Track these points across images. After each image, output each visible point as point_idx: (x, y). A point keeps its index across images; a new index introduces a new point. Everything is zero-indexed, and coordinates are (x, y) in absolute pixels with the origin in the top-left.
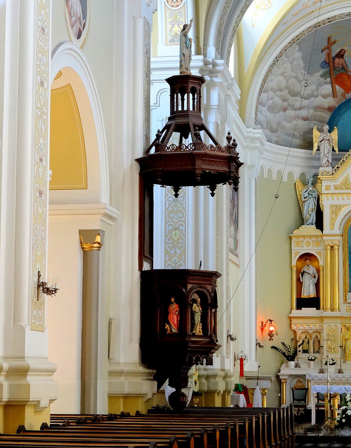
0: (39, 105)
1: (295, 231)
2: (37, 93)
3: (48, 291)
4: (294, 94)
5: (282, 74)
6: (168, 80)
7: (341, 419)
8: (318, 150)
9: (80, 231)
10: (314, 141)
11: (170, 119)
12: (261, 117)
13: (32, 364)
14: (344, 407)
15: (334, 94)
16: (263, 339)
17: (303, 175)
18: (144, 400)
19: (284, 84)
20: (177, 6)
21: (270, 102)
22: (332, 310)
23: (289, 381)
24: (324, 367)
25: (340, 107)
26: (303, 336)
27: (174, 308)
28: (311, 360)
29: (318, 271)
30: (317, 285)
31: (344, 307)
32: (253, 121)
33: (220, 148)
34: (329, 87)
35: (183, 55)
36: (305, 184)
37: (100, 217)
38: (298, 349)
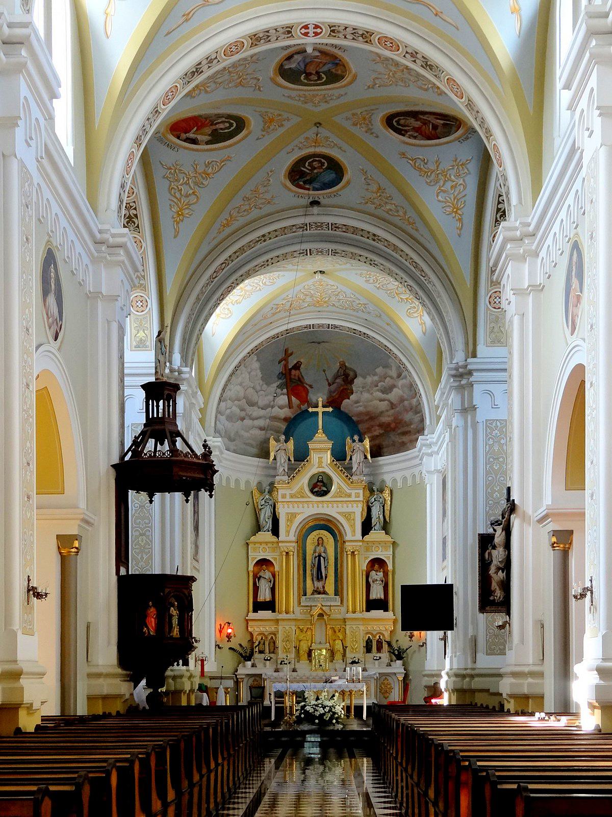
0: (25, 408)
1: (252, 538)
2: (23, 395)
3: (39, 596)
4: (252, 404)
5: (241, 384)
6: (143, 387)
7: (300, 714)
8: (275, 459)
9: (58, 537)
10: (271, 450)
11: (145, 425)
12: (220, 426)
13: (26, 668)
14: (303, 703)
15: (290, 405)
16: (222, 640)
17: (259, 483)
18: (123, 700)
19: (242, 394)
20: (143, 311)
21: (228, 411)
22: (287, 613)
23: (245, 680)
24: (279, 666)
25: (295, 418)
26: (259, 638)
27: (152, 611)
28: (267, 660)
29: (274, 576)
30: (273, 590)
31: (298, 610)
32: (213, 429)
33: (196, 455)
34: (286, 397)
35: (158, 361)
36: (262, 492)
37: (78, 522)
38: (255, 650)
